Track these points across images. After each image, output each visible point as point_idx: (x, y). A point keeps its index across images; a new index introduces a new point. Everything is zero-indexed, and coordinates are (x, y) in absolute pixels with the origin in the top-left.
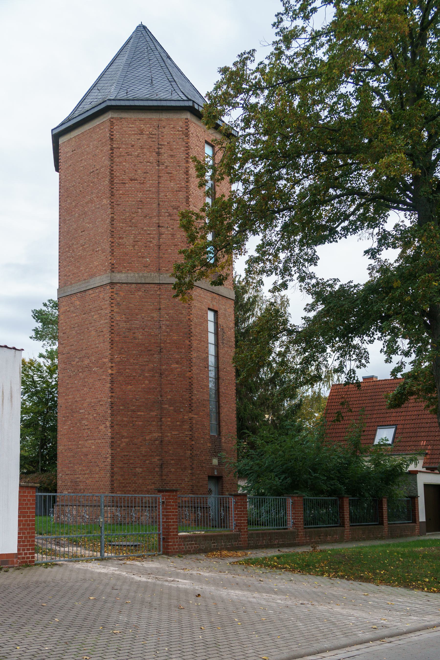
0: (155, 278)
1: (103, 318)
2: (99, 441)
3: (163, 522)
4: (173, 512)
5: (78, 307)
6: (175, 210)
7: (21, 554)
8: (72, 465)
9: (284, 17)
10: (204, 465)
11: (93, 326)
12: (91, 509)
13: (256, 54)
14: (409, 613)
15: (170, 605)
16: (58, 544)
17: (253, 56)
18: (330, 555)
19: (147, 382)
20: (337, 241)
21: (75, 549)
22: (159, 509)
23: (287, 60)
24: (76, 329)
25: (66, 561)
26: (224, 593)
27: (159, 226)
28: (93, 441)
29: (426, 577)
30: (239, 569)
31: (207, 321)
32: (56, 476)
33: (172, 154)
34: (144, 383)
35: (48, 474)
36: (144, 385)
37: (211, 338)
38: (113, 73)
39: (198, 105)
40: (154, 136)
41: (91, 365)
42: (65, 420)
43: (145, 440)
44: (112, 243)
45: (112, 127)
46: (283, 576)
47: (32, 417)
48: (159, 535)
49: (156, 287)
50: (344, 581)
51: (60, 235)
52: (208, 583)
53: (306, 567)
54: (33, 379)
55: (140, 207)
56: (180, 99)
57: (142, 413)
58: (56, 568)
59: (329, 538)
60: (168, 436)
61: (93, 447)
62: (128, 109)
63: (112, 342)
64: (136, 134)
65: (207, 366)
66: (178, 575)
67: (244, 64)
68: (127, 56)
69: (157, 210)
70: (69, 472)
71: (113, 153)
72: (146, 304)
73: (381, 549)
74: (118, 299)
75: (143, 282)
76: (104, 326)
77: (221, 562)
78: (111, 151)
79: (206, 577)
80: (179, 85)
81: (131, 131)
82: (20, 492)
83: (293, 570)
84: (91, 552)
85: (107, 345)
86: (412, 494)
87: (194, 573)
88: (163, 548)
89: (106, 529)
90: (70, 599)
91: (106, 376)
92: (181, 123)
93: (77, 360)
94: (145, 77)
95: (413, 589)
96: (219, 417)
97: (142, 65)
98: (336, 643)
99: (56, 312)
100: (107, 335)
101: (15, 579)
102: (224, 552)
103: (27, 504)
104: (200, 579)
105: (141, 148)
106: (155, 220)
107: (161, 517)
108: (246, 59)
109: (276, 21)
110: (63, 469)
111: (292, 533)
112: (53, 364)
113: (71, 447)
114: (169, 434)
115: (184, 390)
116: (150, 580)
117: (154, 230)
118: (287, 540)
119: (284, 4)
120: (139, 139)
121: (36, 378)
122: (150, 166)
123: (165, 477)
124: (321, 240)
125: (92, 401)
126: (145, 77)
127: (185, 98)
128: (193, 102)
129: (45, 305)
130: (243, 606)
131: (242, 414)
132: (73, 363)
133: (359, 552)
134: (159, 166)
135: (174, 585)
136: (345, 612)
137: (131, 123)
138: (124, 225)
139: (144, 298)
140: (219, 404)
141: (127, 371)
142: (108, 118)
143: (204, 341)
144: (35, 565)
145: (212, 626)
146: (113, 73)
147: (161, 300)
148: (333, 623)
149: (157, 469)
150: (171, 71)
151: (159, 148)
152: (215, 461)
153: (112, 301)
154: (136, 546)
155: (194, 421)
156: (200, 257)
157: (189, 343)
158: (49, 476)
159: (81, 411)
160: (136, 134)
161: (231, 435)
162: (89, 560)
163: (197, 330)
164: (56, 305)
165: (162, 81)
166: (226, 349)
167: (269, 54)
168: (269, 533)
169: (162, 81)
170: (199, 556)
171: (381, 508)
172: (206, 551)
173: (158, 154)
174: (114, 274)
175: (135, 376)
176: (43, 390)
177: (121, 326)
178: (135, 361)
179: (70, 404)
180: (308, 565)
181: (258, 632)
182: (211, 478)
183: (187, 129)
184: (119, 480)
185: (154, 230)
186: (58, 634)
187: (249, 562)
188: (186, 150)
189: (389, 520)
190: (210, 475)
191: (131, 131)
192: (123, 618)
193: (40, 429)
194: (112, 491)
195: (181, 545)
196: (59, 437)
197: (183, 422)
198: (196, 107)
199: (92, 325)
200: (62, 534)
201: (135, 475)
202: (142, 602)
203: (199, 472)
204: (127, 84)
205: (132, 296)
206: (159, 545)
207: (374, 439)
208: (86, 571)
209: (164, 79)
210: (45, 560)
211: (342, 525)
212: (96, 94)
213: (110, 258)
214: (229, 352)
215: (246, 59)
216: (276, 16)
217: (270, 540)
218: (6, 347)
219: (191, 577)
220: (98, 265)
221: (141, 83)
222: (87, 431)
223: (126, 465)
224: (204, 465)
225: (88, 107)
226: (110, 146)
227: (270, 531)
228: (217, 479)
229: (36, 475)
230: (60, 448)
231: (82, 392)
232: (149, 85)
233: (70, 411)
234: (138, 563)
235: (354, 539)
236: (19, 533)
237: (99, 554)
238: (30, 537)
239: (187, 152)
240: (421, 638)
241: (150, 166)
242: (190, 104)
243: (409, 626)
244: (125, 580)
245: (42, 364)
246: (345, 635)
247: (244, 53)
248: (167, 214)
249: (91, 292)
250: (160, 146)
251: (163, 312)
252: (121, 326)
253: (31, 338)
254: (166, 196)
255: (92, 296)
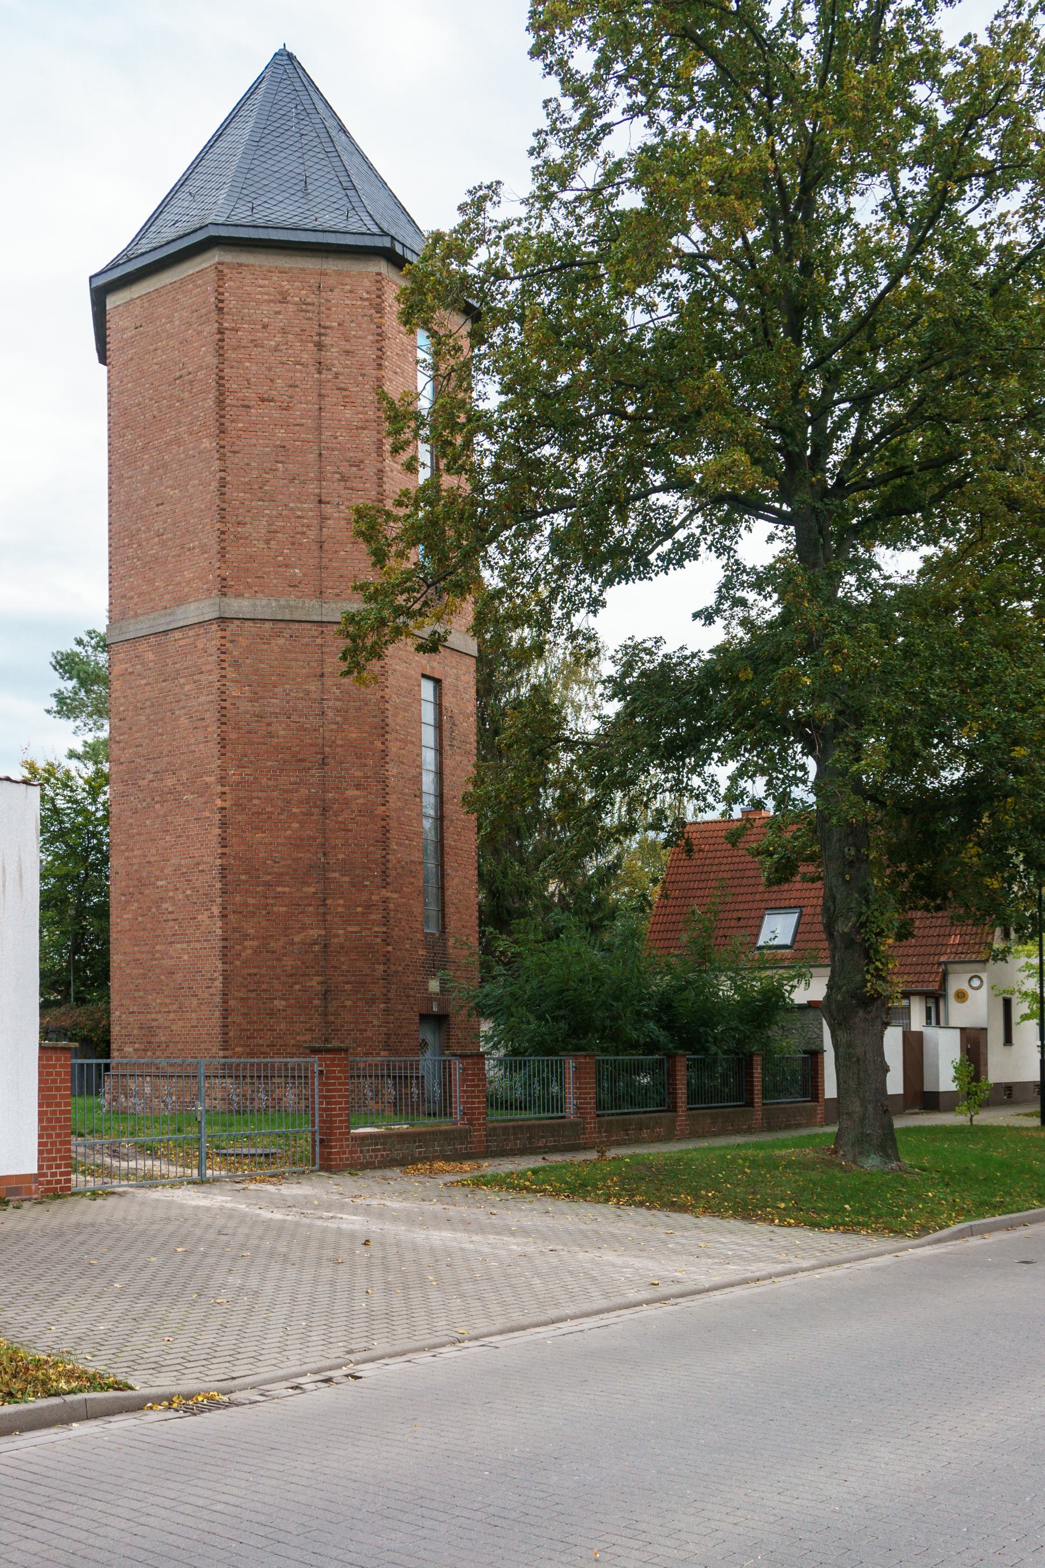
0: (311, 609)
1: (205, 692)
2: (198, 945)
3: (320, 1109)
4: (340, 1090)
5: (151, 665)
6: (355, 469)
7: (45, 1175)
8: (141, 993)
9: (551, 139)
10: (411, 993)
11: (184, 708)
12: (182, 1083)
13: (502, 190)
14: (728, 1260)
15: (319, 1258)
16: (115, 1154)
17: (497, 195)
18: (627, 1165)
19: (296, 825)
20: (650, 579)
21: (149, 1163)
22: (313, 1084)
23: (563, 211)
24: (147, 711)
25: (131, 1186)
26: (420, 1236)
27: (320, 502)
28: (185, 945)
29: (783, 1200)
30: (458, 1194)
31: (419, 700)
32: (108, 1012)
33: (348, 347)
34: (289, 828)
35: (90, 1007)
36: (289, 832)
37: (428, 736)
38: (223, 158)
39: (404, 245)
40: (310, 308)
41: (179, 788)
42: (127, 902)
43: (292, 943)
44: (223, 533)
45: (221, 283)
46: (537, 1205)
47: (53, 886)
48: (313, 1133)
49: (314, 631)
50: (643, 1211)
51: (110, 509)
52: (395, 1220)
53: (578, 1189)
54: (54, 806)
55: (281, 458)
56: (364, 230)
57: (287, 889)
58: (112, 1201)
59: (645, 1133)
60: (338, 936)
61: (186, 957)
62: (256, 246)
63: (223, 742)
64: (271, 301)
65: (419, 794)
66: (342, 1207)
67: (480, 210)
68: (251, 124)
69: (316, 468)
70: (135, 1009)
71: (222, 340)
72: (293, 663)
73: (717, 1153)
74: (235, 653)
75: (288, 617)
76: (206, 707)
77: (430, 1183)
78: (219, 336)
79: (394, 1210)
80: (363, 198)
81: (260, 293)
82: (40, 1059)
83: (556, 1194)
84: (180, 1170)
85: (214, 749)
86: (814, 1047)
87: (375, 1202)
88: (321, 1158)
89: (210, 1123)
90: (141, 1252)
91: (212, 811)
92: (367, 283)
93: (151, 776)
94: (292, 175)
95: (754, 1222)
96: (443, 895)
97: (284, 146)
98: (586, 1307)
99: (103, 658)
100: (213, 728)
101: (36, 1220)
102: (439, 1165)
103: (54, 1081)
104: (382, 1214)
105: (284, 331)
106: (312, 488)
107: (317, 1100)
108: (484, 198)
109: (536, 145)
110: (124, 1002)
111: (574, 1125)
112: (98, 773)
113: (138, 956)
114: (341, 932)
115: (371, 842)
116: (289, 1218)
117: (311, 510)
118: (565, 1138)
119: (548, 114)
120: (278, 313)
121: (60, 803)
122: (301, 372)
123: (332, 1018)
124: (622, 574)
125: (183, 862)
126: (292, 175)
127: (376, 230)
128: (393, 238)
129: (80, 642)
130: (450, 1255)
131: (498, 884)
132: (140, 782)
133: (679, 1160)
134: (320, 373)
135: (333, 1225)
136: (619, 1261)
137: (259, 278)
138: (248, 496)
139: (288, 651)
140: (443, 870)
141: (256, 802)
142: (212, 262)
143: (413, 743)
144: (73, 1194)
145: (388, 1289)
146: (223, 158)
147: (325, 657)
148: (594, 1279)
149: (316, 1002)
150: (346, 163)
151: (320, 335)
152: (434, 985)
153: (223, 656)
154: (267, 1155)
155: (391, 906)
156: (392, 601)
157: (383, 747)
158: (92, 1013)
159: (160, 883)
160: (271, 301)
161: (468, 931)
162: (177, 1183)
163: (399, 720)
164: (104, 645)
165: (327, 186)
166: (458, 758)
167: (527, 195)
168: (529, 1127)
169: (327, 186)
170: (388, 1173)
171: (750, 1075)
172: (402, 1163)
173: (320, 346)
174: (225, 599)
175: (272, 813)
176: (76, 829)
177: (242, 709)
178: (270, 783)
179: (135, 867)
180: (583, 1185)
181: (462, 1296)
182: (426, 1018)
183: (379, 297)
184: (240, 1025)
185: (311, 510)
186: (121, 1306)
187: (480, 1182)
188: (377, 341)
189: (764, 1097)
190: (424, 1012)
191: (260, 293)
192: (235, 1280)
193: (72, 912)
194: (226, 1045)
195: (356, 1152)
196: (113, 936)
197: (369, 906)
198: (399, 249)
199: (181, 704)
200: (123, 1134)
201: (272, 1013)
202: (271, 1254)
203: (400, 1007)
204: (253, 189)
205: (266, 647)
206: (314, 1152)
207: (757, 935)
208: (170, 1204)
209: (332, 183)
210: (91, 1185)
211: (673, 1108)
212: (186, 204)
213: (218, 565)
214: (464, 765)
215: (484, 198)
216: (536, 135)
217: (530, 1138)
218: (8, 779)
219: (367, 1210)
220: (193, 579)
221: (283, 188)
222: (171, 924)
223: (253, 995)
224: (411, 993)
225: (170, 233)
226: (216, 325)
227: (530, 1123)
228: (439, 1021)
229: (63, 1009)
230: (116, 959)
231: (162, 843)
232: (300, 194)
233: (136, 883)
234: (270, 1188)
235: (695, 1134)
236: (40, 1136)
237: (196, 1172)
238: (62, 1143)
239: (379, 346)
240: (730, 1296)
241: (301, 372)
242: (386, 242)
243: (717, 1279)
244: (243, 1218)
245: (74, 773)
246: (606, 1295)
247: (480, 187)
248: (338, 476)
249: (177, 635)
250: (323, 331)
251: (329, 682)
252: (242, 709)
253: (48, 712)
254: (336, 438)
255: (182, 643)
